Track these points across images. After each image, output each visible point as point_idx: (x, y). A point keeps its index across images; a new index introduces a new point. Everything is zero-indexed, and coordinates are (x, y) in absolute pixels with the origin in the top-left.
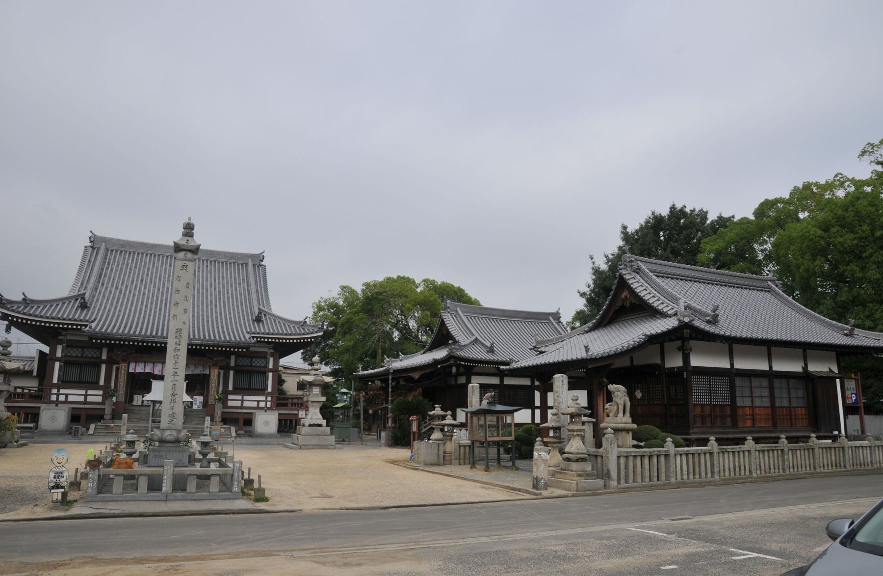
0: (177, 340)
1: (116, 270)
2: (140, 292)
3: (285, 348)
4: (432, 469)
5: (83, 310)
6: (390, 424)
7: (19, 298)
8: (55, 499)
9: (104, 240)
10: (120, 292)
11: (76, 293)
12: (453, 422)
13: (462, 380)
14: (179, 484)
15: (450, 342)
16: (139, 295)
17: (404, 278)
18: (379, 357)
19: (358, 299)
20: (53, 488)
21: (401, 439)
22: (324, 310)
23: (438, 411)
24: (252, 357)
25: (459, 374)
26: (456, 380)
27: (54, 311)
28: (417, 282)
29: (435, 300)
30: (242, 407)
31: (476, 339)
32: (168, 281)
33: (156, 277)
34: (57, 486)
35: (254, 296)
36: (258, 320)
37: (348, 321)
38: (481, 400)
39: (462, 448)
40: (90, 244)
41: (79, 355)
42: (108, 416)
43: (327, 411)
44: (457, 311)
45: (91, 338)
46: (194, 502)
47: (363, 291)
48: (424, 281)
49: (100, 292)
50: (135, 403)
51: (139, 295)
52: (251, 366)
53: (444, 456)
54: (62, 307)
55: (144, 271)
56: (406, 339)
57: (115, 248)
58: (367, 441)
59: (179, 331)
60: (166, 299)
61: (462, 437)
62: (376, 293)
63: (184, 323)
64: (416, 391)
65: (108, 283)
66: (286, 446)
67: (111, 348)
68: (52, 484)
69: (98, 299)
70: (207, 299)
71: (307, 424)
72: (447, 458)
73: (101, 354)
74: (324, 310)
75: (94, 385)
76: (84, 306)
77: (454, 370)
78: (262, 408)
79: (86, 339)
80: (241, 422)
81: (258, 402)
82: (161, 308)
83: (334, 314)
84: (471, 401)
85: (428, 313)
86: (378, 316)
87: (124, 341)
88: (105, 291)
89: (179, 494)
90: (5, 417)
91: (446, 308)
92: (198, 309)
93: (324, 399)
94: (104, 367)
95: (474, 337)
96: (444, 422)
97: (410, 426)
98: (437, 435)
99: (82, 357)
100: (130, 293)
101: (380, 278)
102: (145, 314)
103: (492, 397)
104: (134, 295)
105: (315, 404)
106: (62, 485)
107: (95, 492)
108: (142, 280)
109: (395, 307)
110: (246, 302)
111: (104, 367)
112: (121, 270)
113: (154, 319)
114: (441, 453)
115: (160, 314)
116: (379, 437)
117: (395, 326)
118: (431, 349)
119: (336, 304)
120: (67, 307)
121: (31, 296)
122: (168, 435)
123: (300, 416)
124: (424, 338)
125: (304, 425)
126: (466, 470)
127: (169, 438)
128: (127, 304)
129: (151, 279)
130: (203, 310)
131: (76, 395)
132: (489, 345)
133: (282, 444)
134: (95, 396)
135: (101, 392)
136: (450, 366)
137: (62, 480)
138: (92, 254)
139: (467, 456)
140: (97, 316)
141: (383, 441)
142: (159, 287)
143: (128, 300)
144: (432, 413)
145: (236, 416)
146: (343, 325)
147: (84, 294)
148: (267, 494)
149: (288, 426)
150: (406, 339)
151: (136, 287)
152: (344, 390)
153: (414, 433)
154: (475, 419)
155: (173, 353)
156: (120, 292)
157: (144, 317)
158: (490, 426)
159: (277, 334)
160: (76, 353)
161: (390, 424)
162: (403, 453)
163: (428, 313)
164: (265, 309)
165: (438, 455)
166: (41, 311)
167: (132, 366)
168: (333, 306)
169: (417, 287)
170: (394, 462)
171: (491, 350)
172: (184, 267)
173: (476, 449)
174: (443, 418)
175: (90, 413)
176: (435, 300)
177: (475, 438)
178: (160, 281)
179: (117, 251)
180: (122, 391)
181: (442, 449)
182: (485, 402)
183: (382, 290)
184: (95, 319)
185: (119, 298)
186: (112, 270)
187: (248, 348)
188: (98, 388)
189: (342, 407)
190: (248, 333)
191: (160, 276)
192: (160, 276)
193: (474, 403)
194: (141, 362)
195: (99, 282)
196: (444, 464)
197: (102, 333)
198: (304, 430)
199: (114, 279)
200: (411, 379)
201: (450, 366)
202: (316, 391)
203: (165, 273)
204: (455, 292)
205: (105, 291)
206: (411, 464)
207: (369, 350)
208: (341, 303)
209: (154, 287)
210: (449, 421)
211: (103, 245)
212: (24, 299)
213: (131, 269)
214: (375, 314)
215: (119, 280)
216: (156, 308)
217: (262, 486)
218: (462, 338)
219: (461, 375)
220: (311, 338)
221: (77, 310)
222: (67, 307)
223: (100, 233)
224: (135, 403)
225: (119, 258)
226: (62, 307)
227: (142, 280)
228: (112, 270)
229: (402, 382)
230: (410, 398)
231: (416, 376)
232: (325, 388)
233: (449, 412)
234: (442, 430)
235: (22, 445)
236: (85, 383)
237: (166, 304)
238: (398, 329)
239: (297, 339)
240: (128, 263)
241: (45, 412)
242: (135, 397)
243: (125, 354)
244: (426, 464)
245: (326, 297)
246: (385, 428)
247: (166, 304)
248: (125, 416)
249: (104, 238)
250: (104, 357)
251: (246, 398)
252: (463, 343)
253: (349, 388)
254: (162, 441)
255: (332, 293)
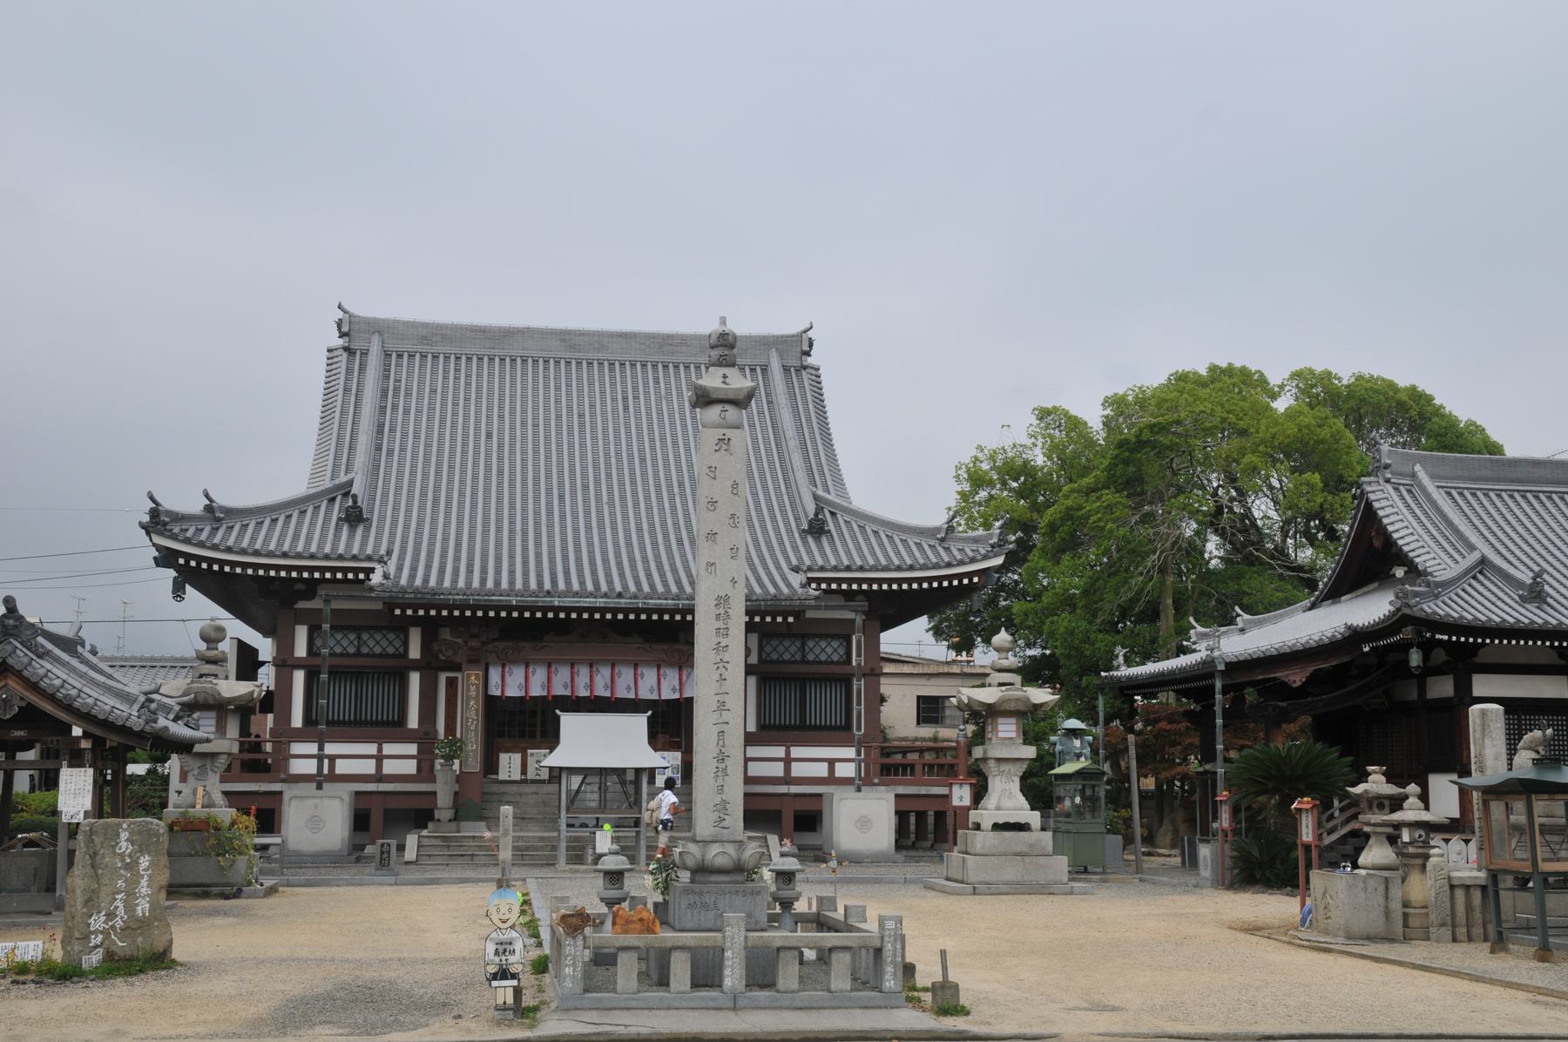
0: (720, 624)
1: (419, 411)
2: (488, 469)
3: (893, 606)
4: (1371, 949)
5: (353, 528)
6: (1225, 820)
7: (196, 506)
8: (500, 1001)
9: (378, 328)
10: (438, 473)
11: (328, 484)
12: (1425, 816)
13: (1442, 688)
14: (761, 974)
15: (1399, 572)
16: (487, 478)
17: (1229, 371)
18: (1167, 621)
19: (1091, 443)
20: (495, 977)
21: (1267, 864)
22: (991, 484)
23: (1376, 783)
24: (805, 637)
25: (1430, 670)
26: (1422, 689)
27: (283, 535)
28: (1274, 380)
29: (1336, 437)
30: (787, 779)
31: (1483, 561)
32: (559, 433)
33: (524, 424)
34: (503, 974)
35: (797, 460)
36: (817, 529)
37: (1069, 514)
38: (1512, 751)
39: (1460, 894)
40: (341, 342)
41: (351, 650)
42: (444, 811)
43: (1039, 787)
44: (1413, 475)
45: (390, 605)
46: (798, 1013)
47: (1107, 423)
48: (1297, 375)
49: (387, 474)
50: (503, 776)
51: (487, 478)
52: (804, 661)
53: (1406, 916)
54: (300, 523)
55: (490, 409)
56: (1250, 561)
57: (406, 346)
58: (1154, 871)
59: (723, 601)
60: (561, 485)
61: (1458, 860)
62: (1151, 427)
63: (734, 581)
64: (1293, 720)
65: (403, 449)
66: (929, 887)
67: (431, 629)
68: (492, 969)
69: (385, 495)
70: (668, 479)
71: (987, 824)
72: (1413, 922)
73: (406, 644)
74: (991, 484)
75: (393, 727)
76: (354, 518)
77: (1415, 658)
78: (846, 781)
79: (378, 606)
80: (788, 820)
81: (831, 763)
82: (550, 512)
83: (1020, 494)
84: (1480, 756)
85: (1316, 478)
86: (1159, 497)
87: (474, 608)
88: (400, 473)
89: (762, 995)
90: (227, 821)
91: (1378, 468)
92: (649, 508)
93: (1030, 752)
94: (415, 679)
95: (1476, 556)
96: (1397, 816)
97: (1295, 829)
98: (1376, 854)
99: (358, 654)
100: (463, 472)
101: (1154, 376)
102: (512, 531)
103: (1547, 742)
104: (475, 477)
105: (1005, 767)
106: (513, 970)
107: (579, 990)
108: (489, 435)
109: (1207, 463)
110: (775, 478)
111: (415, 679)
112: (431, 408)
113: (538, 544)
114: (1396, 906)
115: (550, 526)
116: (1191, 862)
117: (1214, 520)
118: (1335, 593)
119: (1026, 462)
120: (312, 524)
121: (223, 499)
122: (718, 855)
123: (956, 802)
124: (1305, 555)
125: (978, 827)
126: (1478, 957)
127: (721, 861)
128: (461, 504)
129: (512, 428)
130: (662, 509)
131: (354, 757)
132: (1526, 577)
133: (915, 882)
134: (401, 759)
135: (412, 749)
136: (1405, 647)
137: (512, 959)
138: (349, 371)
139: (1478, 915)
140: (391, 542)
141: (1205, 872)
142: (536, 452)
143: (462, 494)
144: (1358, 789)
145: (772, 805)
146: (1053, 528)
147: (350, 483)
148: (964, 1000)
149: (925, 832)
150: (1250, 561)
151: (476, 454)
152: (1074, 723)
153: (1307, 847)
154: (1497, 808)
155: (714, 657)
156: (438, 473)
157: (512, 539)
158: (1545, 830)
159: (874, 569)
160: (345, 643)
161: (1225, 820)
162: (1278, 907)
163: (1316, 478)
164: (832, 497)
165: (1387, 913)
166: (253, 539)
167: (495, 675)
168: (1015, 469)
169: (1274, 396)
170: (1253, 929)
171: (1535, 594)
172: (724, 441)
173: (1506, 898)
174: (1397, 803)
175: (393, 804)
176: (1336, 437)
177: (1504, 861)
178: (536, 434)
179: (411, 356)
180: (474, 746)
181: (1396, 893)
182: (1524, 758)
183: (1169, 417)
184: (389, 553)
185: (437, 489)
186: (407, 412)
187: (798, 614)
188: (407, 737)
189: (1079, 774)
190: (796, 570)
191: (535, 417)
192: (535, 417)
193: (1489, 763)
194: (516, 662)
195: (379, 448)
196: (1406, 939)
197: (417, 591)
198: (983, 840)
199: (416, 436)
200: (1282, 689)
201: (1405, 647)
202: (1007, 729)
203: (547, 409)
204: (1401, 405)
205: (400, 473)
206: (1310, 934)
207: (1134, 601)
208: (1040, 460)
209: (524, 452)
210: (1411, 812)
211: (376, 340)
212: (209, 509)
213: (455, 404)
214: (1149, 489)
215: (429, 435)
216: (537, 513)
217: (952, 977)
218: (1437, 561)
219: (1438, 671)
220: (970, 575)
221: (338, 529)
222: (312, 524)
223: (368, 307)
224: (503, 776)
225: (422, 376)
226: (300, 523)
227: (489, 435)
228: (407, 412)
229: (1250, 696)
230: (1280, 744)
231: (1296, 677)
232: (1035, 723)
233: (1413, 788)
234: (1393, 840)
235: (272, 891)
236: (366, 723)
237: (561, 497)
238: (1221, 533)
239: (930, 580)
240: (445, 387)
241: (294, 803)
242: (504, 758)
243: (474, 643)
244: (1351, 937)
245: (992, 443)
246: (1207, 835)
247: (561, 497)
248: (507, 810)
249: (376, 321)
250: (415, 653)
251: (797, 752)
252: (1442, 576)
253: (1088, 714)
254: (702, 870)
255: (1013, 431)
